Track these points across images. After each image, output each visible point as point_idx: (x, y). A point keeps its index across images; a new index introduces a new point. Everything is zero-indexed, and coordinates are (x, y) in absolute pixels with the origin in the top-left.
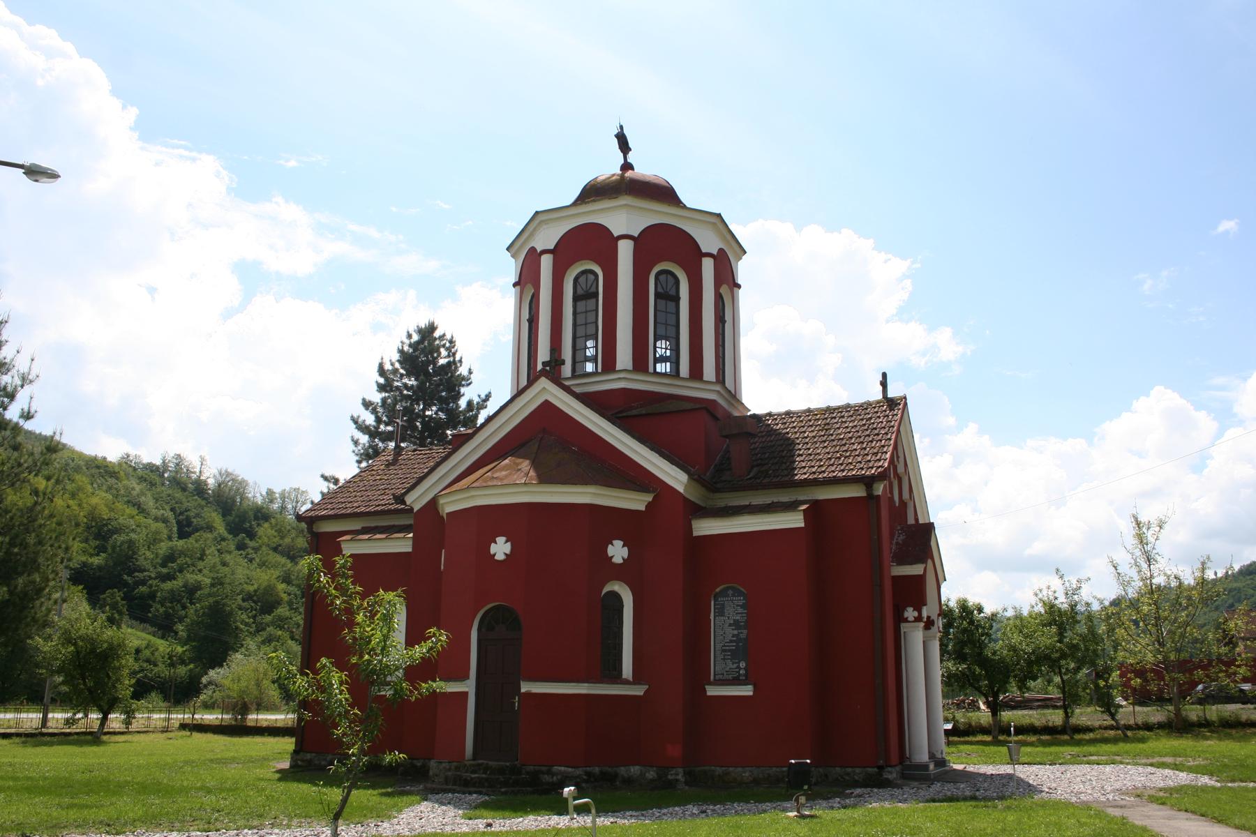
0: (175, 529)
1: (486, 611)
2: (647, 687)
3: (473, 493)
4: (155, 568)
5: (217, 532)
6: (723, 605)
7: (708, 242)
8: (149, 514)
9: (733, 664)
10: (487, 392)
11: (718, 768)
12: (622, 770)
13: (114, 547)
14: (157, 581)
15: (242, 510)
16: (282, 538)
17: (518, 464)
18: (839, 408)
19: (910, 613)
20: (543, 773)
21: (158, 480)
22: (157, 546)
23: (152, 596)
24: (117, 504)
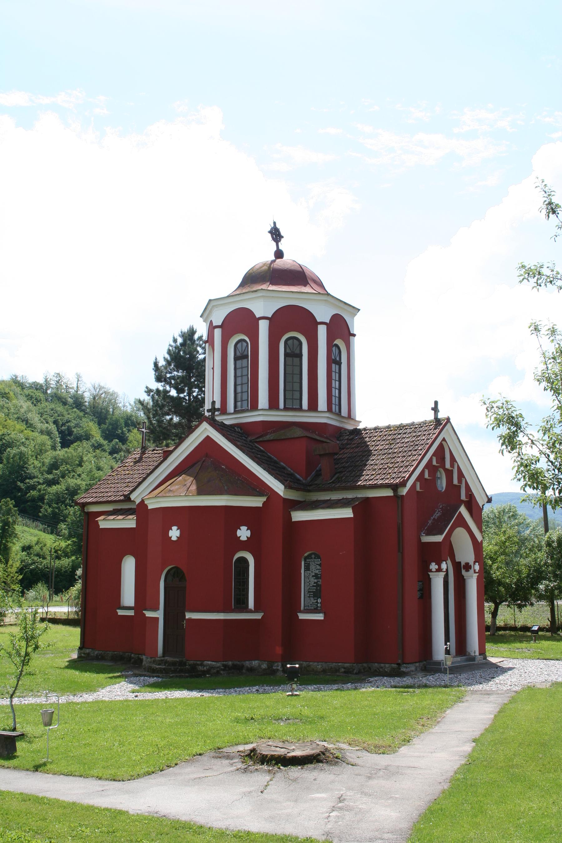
0: (58, 440)
1: (169, 570)
2: (263, 614)
3: (159, 500)
4: (43, 475)
5: (94, 439)
6: (309, 563)
8: (35, 428)
9: (314, 599)
13: (8, 459)
14: (45, 485)
15: (114, 419)
18: (406, 426)
21: (42, 396)
22: (43, 457)
23: (41, 498)
24: (9, 421)
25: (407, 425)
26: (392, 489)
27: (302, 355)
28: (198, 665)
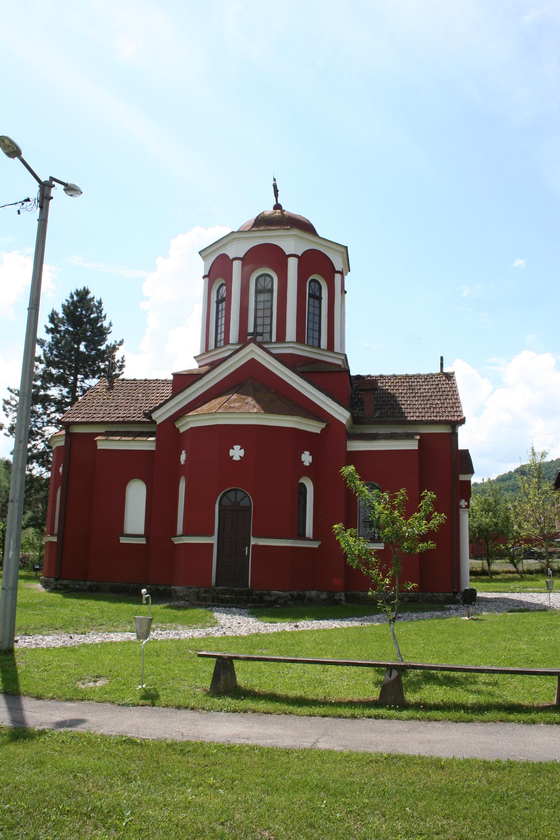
2: (321, 542)
3: (218, 416)
10: (121, 340)
11: (362, 593)
12: (307, 593)
17: (244, 399)
19: (463, 503)
20: (265, 595)
25: (413, 376)
28: (265, 595)
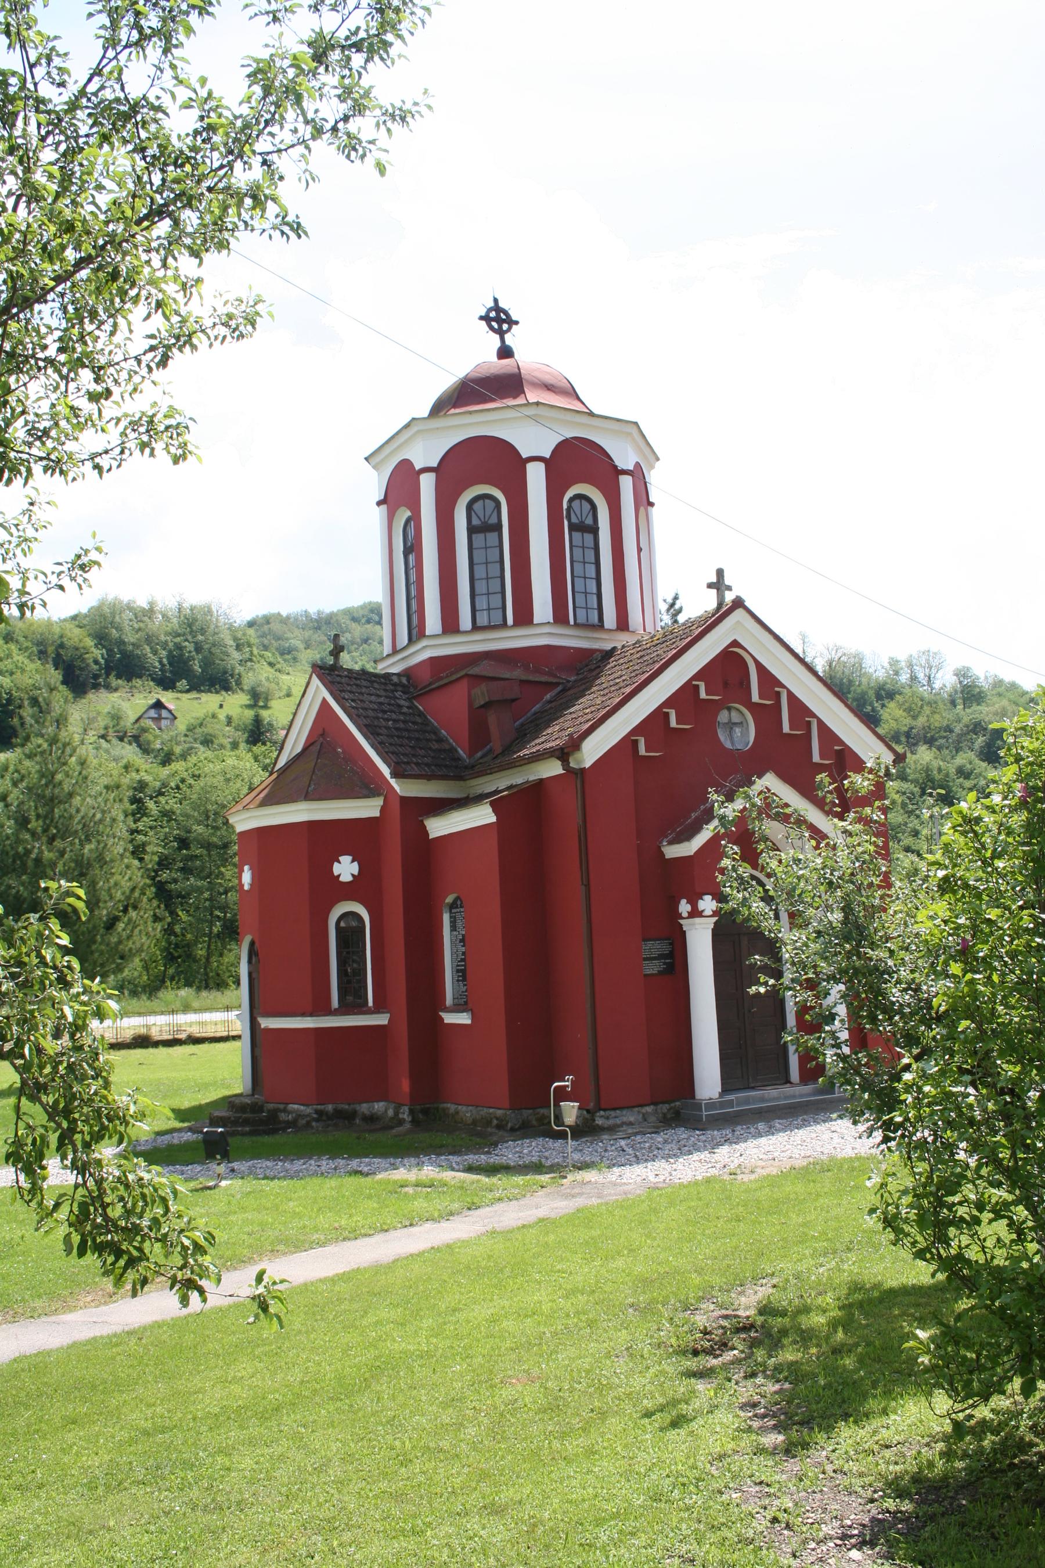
7: (624, 457)
16: (915, 717)
26: (558, 758)
27: (598, 529)
